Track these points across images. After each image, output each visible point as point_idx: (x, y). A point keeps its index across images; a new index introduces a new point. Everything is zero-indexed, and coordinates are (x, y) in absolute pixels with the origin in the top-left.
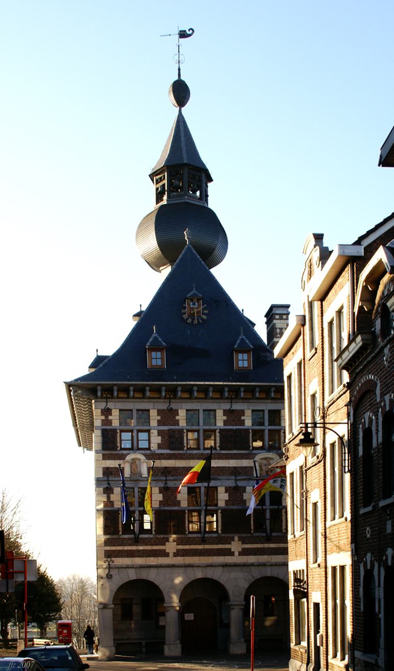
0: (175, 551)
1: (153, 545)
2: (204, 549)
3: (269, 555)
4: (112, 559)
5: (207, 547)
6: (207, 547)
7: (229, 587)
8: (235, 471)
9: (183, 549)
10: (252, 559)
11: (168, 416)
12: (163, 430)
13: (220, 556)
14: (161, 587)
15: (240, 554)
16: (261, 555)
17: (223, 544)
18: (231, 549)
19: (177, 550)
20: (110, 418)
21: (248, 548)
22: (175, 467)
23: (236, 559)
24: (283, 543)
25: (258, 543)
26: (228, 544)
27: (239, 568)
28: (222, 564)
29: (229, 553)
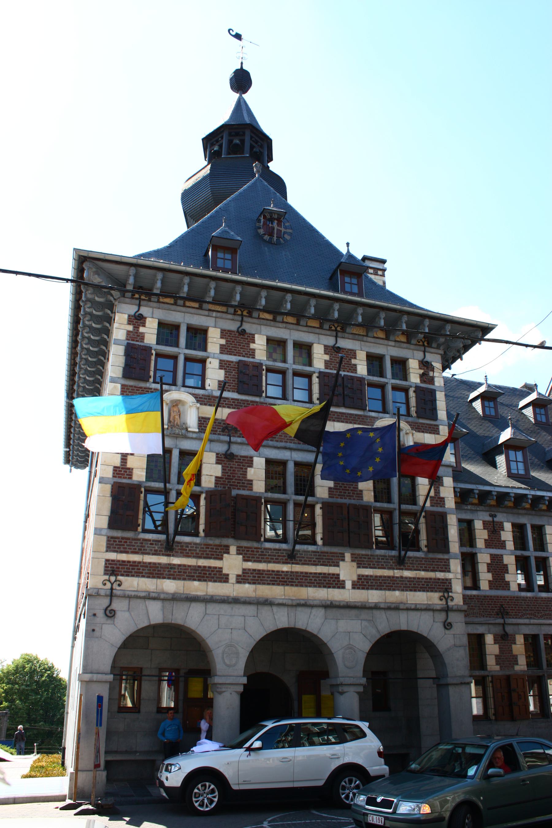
0: (240, 573)
1: (200, 557)
3: (403, 590)
4: (120, 578)
9: (254, 570)
10: (374, 596)
11: (237, 341)
12: (228, 361)
15: (355, 586)
16: (389, 590)
17: (326, 565)
18: (338, 575)
19: (244, 570)
20: (142, 329)
23: (348, 594)
24: (423, 570)
25: (384, 568)
27: (354, 612)
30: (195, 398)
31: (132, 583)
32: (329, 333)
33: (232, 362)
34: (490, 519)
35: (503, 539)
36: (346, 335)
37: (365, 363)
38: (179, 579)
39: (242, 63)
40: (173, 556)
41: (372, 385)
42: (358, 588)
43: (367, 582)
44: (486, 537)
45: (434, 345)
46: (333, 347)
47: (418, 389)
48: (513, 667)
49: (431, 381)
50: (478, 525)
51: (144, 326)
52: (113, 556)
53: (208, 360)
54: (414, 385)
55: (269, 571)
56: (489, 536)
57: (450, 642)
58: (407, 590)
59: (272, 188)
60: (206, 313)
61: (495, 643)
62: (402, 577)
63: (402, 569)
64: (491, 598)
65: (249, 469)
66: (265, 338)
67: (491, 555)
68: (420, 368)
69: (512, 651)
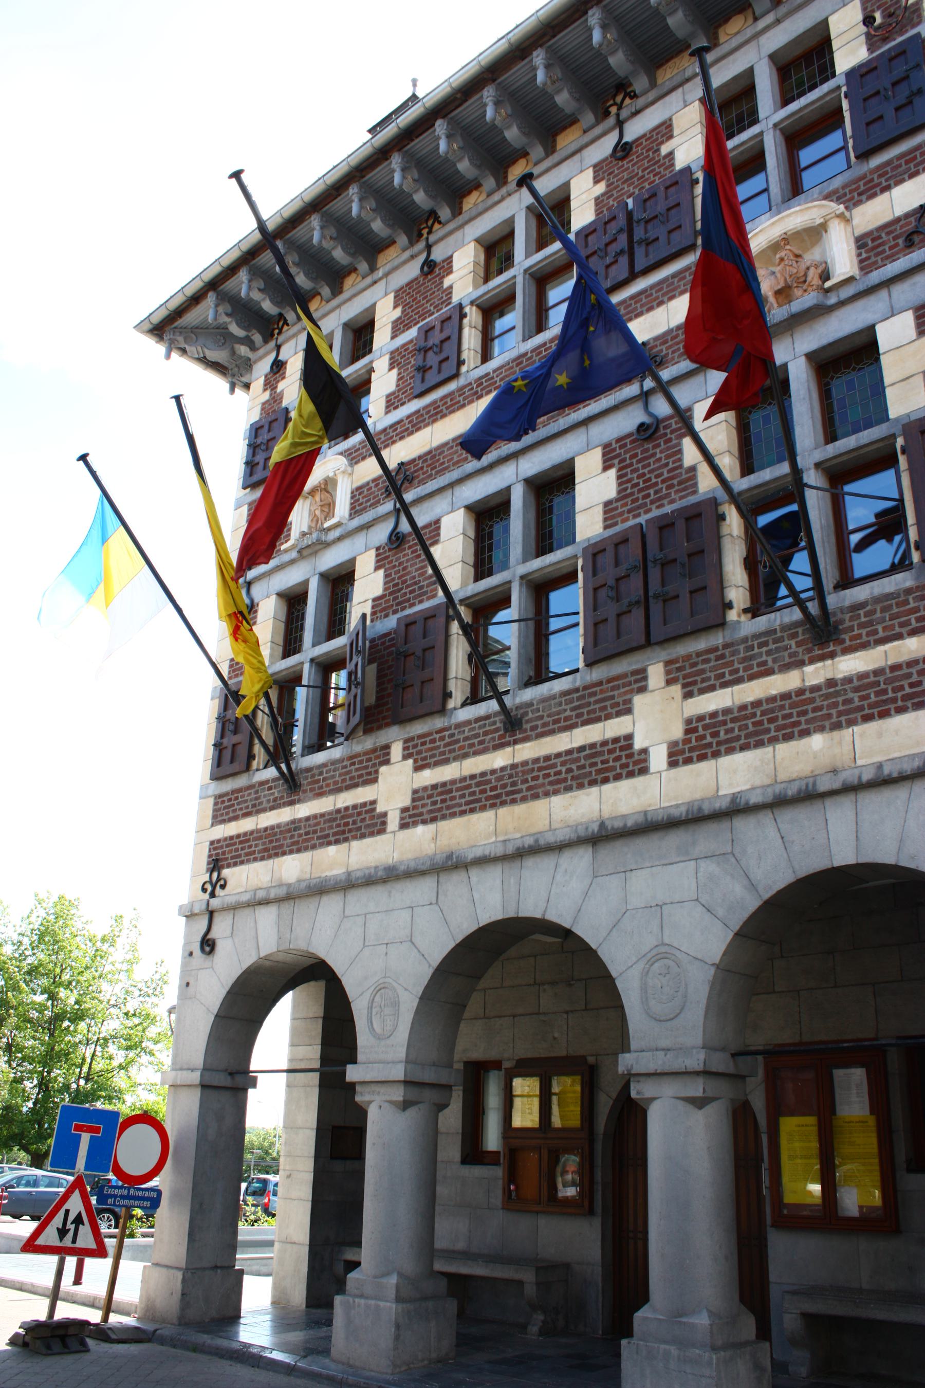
2: (514, 766)
3: (837, 726)
5: (527, 751)
6: (527, 751)
7: (621, 958)
10: (738, 773)
13: (581, 786)
15: (679, 756)
16: (788, 738)
17: (598, 720)
25: (769, 672)
26: (619, 714)
28: (582, 832)
29: (623, 760)
43: (715, 734)
62: (831, 683)
63: (832, 655)
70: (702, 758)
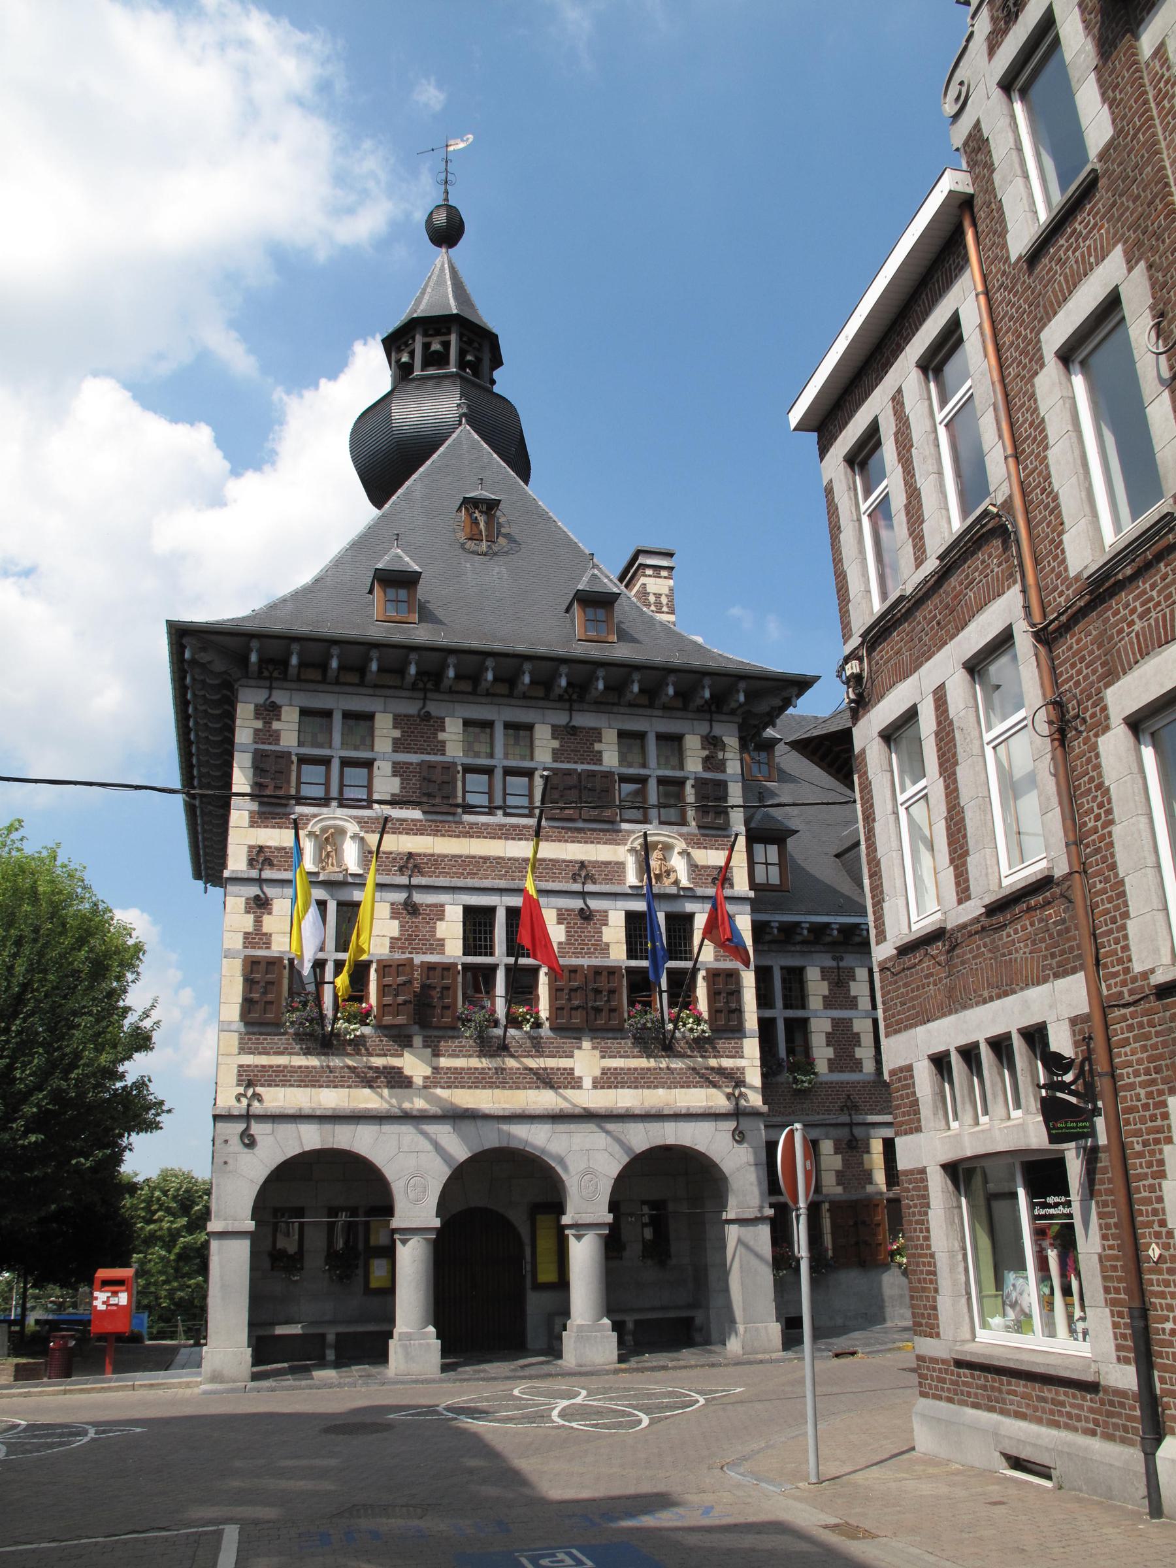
3: (669, 1088)
4: (259, 1090)
8: (582, 871)
12: (405, 763)
14: (389, 1173)
15: (598, 1084)
17: (555, 1057)
18: (572, 1069)
20: (276, 725)
21: (616, 1069)
22: (433, 855)
23: (589, 1098)
28: (551, 1112)
30: (359, 823)
31: (277, 1098)
32: (558, 705)
33: (411, 764)
34: (834, 964)
35: (853, 993)
36: (586, 707)
37: (616, 747)
38: (342, 1087)
39: (446, 192)
40: (333, 1055)
41: (624, 779)
42: (602, 1088)
44: (827, 993)
45: (725, 709)
46: (566, 726)
47: (700, 783)
48: (864, 1187)
49: (721, 766)
50: (813, 974)
51: (279, 720)
52: (248, 1060)
53: (376, 764)
54: (693, 776)
55: (470, 1069)
56: (830, 990)
57: (737, 1161)
58: (676, 1087)
59: (485, 446)
60: (370, 691)
61: (836, 1153)
64: (830, 1085)
65: (438, 923)
66: (461, 721)
67: (833, 1019)
68: (703, 748)
69: (862, 1163)
70: (609, 1087)
